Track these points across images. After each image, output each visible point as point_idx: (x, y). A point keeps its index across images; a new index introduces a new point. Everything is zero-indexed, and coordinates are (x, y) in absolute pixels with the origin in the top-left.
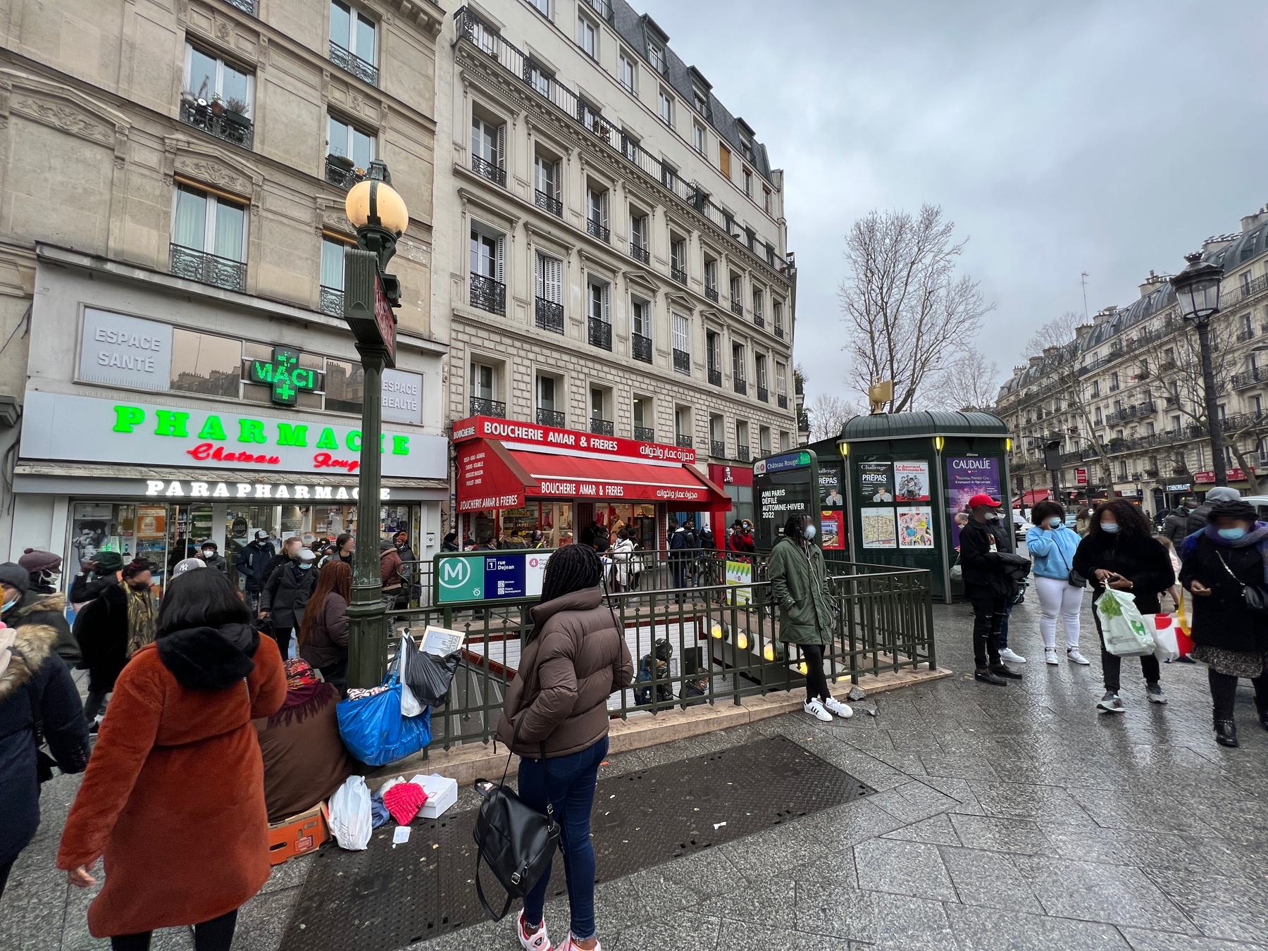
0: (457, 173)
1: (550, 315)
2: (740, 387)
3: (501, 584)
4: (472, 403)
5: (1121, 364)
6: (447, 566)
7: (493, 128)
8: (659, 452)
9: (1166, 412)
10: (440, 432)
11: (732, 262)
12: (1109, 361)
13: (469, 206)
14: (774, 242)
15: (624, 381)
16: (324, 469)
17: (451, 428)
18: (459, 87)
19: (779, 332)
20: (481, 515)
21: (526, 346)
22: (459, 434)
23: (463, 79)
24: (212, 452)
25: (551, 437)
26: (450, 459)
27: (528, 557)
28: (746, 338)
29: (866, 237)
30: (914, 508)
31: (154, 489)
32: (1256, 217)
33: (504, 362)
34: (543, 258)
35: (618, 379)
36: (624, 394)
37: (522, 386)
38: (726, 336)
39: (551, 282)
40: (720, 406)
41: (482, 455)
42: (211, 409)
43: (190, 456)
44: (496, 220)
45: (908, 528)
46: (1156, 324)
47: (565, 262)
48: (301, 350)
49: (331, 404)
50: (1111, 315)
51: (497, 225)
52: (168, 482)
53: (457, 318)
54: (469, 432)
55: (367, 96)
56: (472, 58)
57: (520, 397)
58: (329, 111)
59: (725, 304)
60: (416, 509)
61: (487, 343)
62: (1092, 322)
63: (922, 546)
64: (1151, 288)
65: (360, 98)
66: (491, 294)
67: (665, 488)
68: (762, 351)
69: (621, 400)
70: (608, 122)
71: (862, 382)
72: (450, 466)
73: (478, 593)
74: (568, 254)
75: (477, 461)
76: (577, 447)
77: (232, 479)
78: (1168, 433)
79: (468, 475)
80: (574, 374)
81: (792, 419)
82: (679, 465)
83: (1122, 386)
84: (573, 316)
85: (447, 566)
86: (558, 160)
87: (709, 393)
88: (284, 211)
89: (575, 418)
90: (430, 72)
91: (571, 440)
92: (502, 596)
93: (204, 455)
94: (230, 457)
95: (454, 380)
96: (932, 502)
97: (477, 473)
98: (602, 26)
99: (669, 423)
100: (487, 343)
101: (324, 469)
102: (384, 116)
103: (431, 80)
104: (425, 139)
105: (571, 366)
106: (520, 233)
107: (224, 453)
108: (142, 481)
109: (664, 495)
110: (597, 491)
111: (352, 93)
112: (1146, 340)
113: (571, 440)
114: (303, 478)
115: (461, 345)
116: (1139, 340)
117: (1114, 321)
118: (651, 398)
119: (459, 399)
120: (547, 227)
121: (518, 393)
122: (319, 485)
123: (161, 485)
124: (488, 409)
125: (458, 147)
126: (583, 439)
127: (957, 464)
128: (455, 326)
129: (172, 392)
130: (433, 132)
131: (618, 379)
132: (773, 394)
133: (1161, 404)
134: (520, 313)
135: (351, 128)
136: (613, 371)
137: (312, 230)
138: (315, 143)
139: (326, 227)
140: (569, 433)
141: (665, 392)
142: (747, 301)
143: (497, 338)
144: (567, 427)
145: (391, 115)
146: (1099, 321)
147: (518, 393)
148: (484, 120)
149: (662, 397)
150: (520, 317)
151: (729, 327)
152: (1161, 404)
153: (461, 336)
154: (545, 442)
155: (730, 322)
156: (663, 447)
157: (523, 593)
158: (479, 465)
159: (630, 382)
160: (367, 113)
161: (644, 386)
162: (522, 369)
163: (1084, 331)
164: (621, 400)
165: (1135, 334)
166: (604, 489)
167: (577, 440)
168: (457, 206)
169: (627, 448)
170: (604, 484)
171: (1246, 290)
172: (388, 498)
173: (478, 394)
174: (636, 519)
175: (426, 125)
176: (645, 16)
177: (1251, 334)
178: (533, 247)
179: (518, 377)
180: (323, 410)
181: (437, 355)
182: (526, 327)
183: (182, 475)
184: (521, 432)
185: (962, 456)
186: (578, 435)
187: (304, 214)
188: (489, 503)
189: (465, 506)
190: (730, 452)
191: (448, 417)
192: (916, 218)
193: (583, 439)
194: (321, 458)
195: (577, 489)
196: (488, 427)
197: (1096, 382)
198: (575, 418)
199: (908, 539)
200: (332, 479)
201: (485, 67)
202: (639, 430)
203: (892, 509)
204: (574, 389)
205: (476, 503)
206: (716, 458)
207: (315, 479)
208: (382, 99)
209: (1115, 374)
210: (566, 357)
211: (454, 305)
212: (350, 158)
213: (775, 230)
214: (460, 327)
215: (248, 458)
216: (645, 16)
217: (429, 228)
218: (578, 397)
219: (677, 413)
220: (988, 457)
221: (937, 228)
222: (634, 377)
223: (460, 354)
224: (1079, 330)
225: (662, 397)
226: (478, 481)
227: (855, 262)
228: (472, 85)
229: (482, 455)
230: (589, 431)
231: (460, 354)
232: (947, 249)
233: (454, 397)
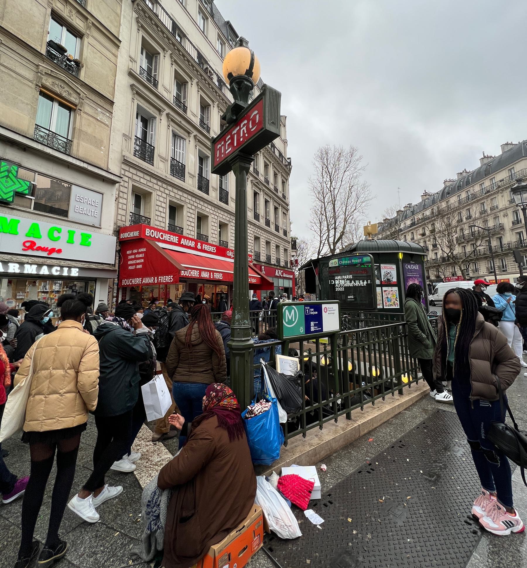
0: (131, 74)
1: (178, 170)
2: (268, 223)
5: (415, 228)
7: (151, 56)
9: (432, 251)
10: (111, 232)
11: (265, 157)
12: (411, 227)
13: (136, 96)
14: (282, 151)
15: (215, 213)
16: (30, 252)
17: (118, 232)
18: (135, 26)
19: (284, 197)
20: (133, 289)
21: (164, 186)
22: (125, 236)
23: (138, 22)
27: (324, 306)
28: (270, 197)
29: (324, 156)
30: (390, 288)
32: (461, 173)
33: (151, 193)
34: (175, 135)
35: (211, 212)
36: (214, 220)
37: (161, 209)
38: (262, 195)
39: (178, 151)
40: (260, 233)
44: (151, 107)
45: (387, 298)
46: (428, 213)
47: (187, 141)
48: (20, 166)
49: (38, 207)
50: (410, 207)
51: (152, 111)
53: (126, 162)
55: (78, 12)
56: (144, 12)
57: (158, 214)
58: (52, 14)
59: (262, 178)
60: (90, 283)
61: (142, 180)
62: (403, 209)
63: (394, 307)
64: (425, 197)
65: (74, 12)
66: (146, 151)
68: (277, 206)
70: (213, 70)
71: (315, 227)
74: (189, 136)
75: (139, 253)
78: (433, 260)
79: (129, 263)
80: (189, 206)
81: (289, 242)
83: (415, 238)
84: (190, 172)
85: (287, 311)
86: (185, 83)
87: (254, 225)
88: (13, 68)
89: (189, 232)
90: (119, 12)
95: (121, 200)
96: (398, 284)
98: (209, 19)
100: (142, 180)
101: (30, 252)
102: (88, 28)
103: (119, 16)
104: (114, 50)
105: (188, 201)
106: (164, 117)
110: (210, 275)
111: (69, 7)
112: (424, 219)
114: (15, 258)
115: (126, 179)
116: (422, 219)
117: (412, 209)
118: (227, 224)
119: (123, 213)
120: (179, 119)
122: (28, 263)
124: (139, 221)
125: (132, 60)
127: (407, 267)
128: (124, 166)
130: (118, 47)
131: (211, 212)
132: (282, 228)
133: (430, 247)
134: (161, 165)
135: (65, 29)
136: (210, 207)
137: (33, 86)
138: (41, 30)
139: (44, 87)
142: (271, 179)
143: (148, 178)
145: (93, 29)
146: (406, 209)
148: (146, 49)
150: (161, 168)
151: (263, 190)
152: (430, 247)
153: (127, 174)
155: (264, 188)
159: (217, 214)
160: (78, 23)
161: (224, 217)
162: (162, 199)
163: (399, 213)
165: (420, 216)
166: (213, 274)
168: (129, 94)
170: (214, 272)
171: (460, 202)
172: (77, 275)
174: (217, 294)
175: (115, 41)
176: (228, 22)
177: (462, 220)
178: (171, 128)
179: (159, 203)
180: (32, 210)
181: (113, 183)
182: (165, 174)
185: (409, 263)
187: (29, 74)
188: (148, 280)
189: (126, 282)
190: (263, 258)
191: (115, 224)
192: (347, 149)
194: (28, 244)
195: (200, 274)
197: (405, 236)
198: (189, 232)
199: (388, 304)
201: (151, 19)
203: (380, 288)
204: (189, 215)
205: (137, 281)
206: (257, 261)
207: (24, 259)
208: (89, 17)
209: (413, 233)
210: (185, 195)
211: (124, 154)
212: (63, 44)
213: (283, 145)
214: (127, 168)
216: (228, 22)
217: (112, 103)
220: (418, 264)
221: (355, 158)
222: (219, 211)
223: (126, 185)
224: (398, 212)
226: (140, 266)
227: (317, 167)
228: (142, 27)
229: (144, 250)
231: (126, 185)
232: (359, 167)
233: (120, 212)
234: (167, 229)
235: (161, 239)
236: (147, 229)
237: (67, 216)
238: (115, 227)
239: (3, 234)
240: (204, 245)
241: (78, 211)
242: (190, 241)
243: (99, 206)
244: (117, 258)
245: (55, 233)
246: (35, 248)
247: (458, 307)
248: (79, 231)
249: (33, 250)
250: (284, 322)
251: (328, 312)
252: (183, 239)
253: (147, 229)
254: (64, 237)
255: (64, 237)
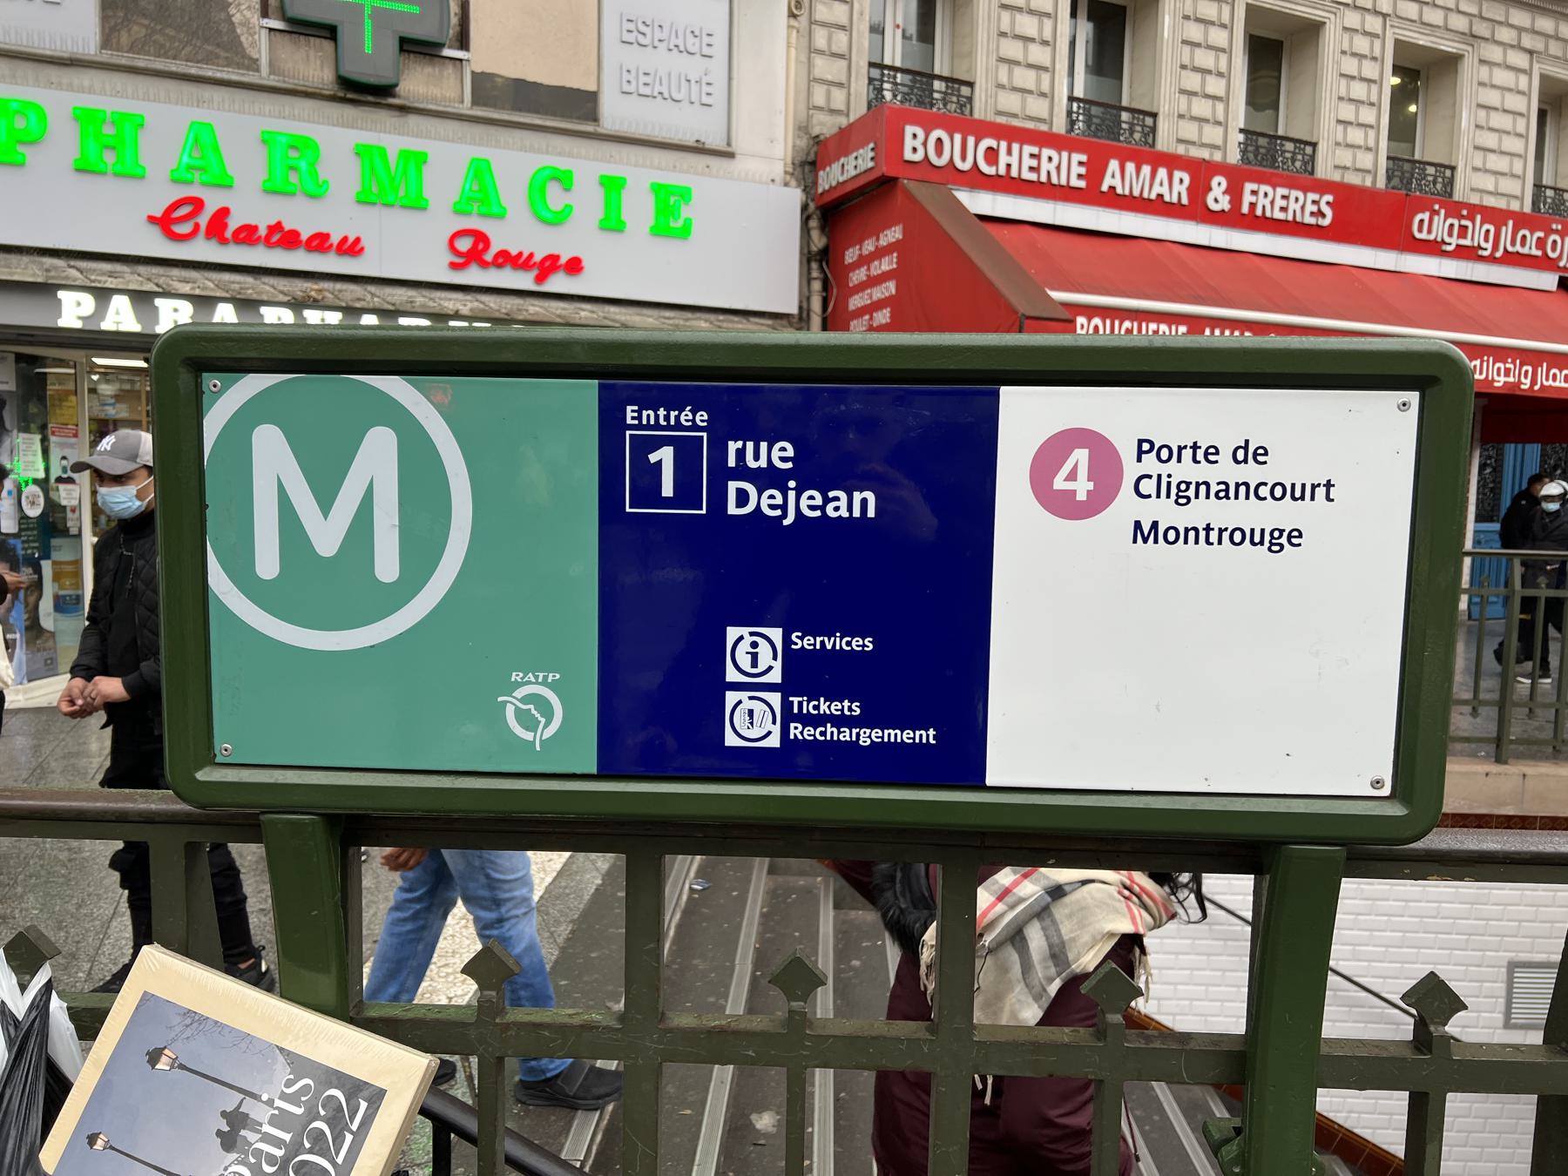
3: (754, 651)
4: (875, 86)
6: (271, 451)
8: (1479, 233)
10: (778, 169)
16: (474, 276)
22: (834, 176)
24: (203, 220)
25: (1112, 177)
26: (807, 257)
27: (1026, 417)
31: (73, 310)
36: (1362, 44)
41: (894, 234)
42: (199, 103)
43: (155, 232)
52: (103, 295)
54: (857, 164)
67: (1500, 353)
69: (1350, 65)
72: (806, 279)
73: (544, 719)
75: (880, 253)
76: (1195, 210)
77: (250, 294)
82: (1549, 281)
85: (271, 451)
91: (1177, 187)
92: (755, 764)
93: (184, 229)
94: (247, 235)
97: (879, 293)
99: (1515, 145)
101: (474, 276)
107: (233, 223)
108: (46, 290)
109: (1497, 375)
113: (1177, 187)
119: (835, 70)
121: (1012, 49)
123: (88, 303)
124: (927, 91)
126: (1219, 184)
129: (107, 56)
140: (1172, 162)
141: (1505, 35)
144: (1164, 143)
147: (1012, 49)
149: (1495, 53)
154: (1093, 195)
156: (1495, 217)
157: (962, 754)
158: (887, 264)
164: (1350, 65)
167: (1199, 189)
169: (1366, 216)
173: (894, 54)
183: (136, 279)
184: (1017, 160)
186: (1201, 172)
191: (803, 128)
193: (1219, 184)
194: (464, 244)
196: (915, 143)
200: (492, 302)
202: (1400, 166)
215: (290, 240)
218: (1205, 59)
219: (1542, 114)
225: (1495, 53)
229: (894, 234)
230: (1234, 157)
233: (822, 67)
234: (1060, 126)
235: (987, 169)
236: (909, 130)
237: (594, 118)
238: (803, 143)
239: (385, 211)
240: (1249, 187)
241: (632, 88)
242: (1162, 173)
243: (720, 50)
244: (817, 286)
245: (554, 189)
246: (489, 257)
247: (1518, 668)
248: (641, 175)
249: (484, 265)
250: (218, 580)
251: (1126, 508)
252: (1114, 165)
253: (909, 130)
254: (586, 203)
255: (586, 203)
